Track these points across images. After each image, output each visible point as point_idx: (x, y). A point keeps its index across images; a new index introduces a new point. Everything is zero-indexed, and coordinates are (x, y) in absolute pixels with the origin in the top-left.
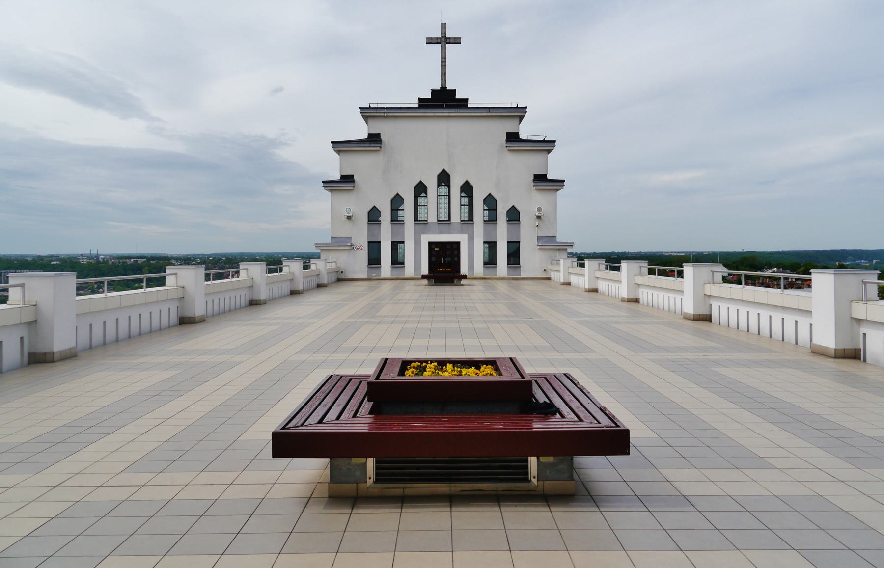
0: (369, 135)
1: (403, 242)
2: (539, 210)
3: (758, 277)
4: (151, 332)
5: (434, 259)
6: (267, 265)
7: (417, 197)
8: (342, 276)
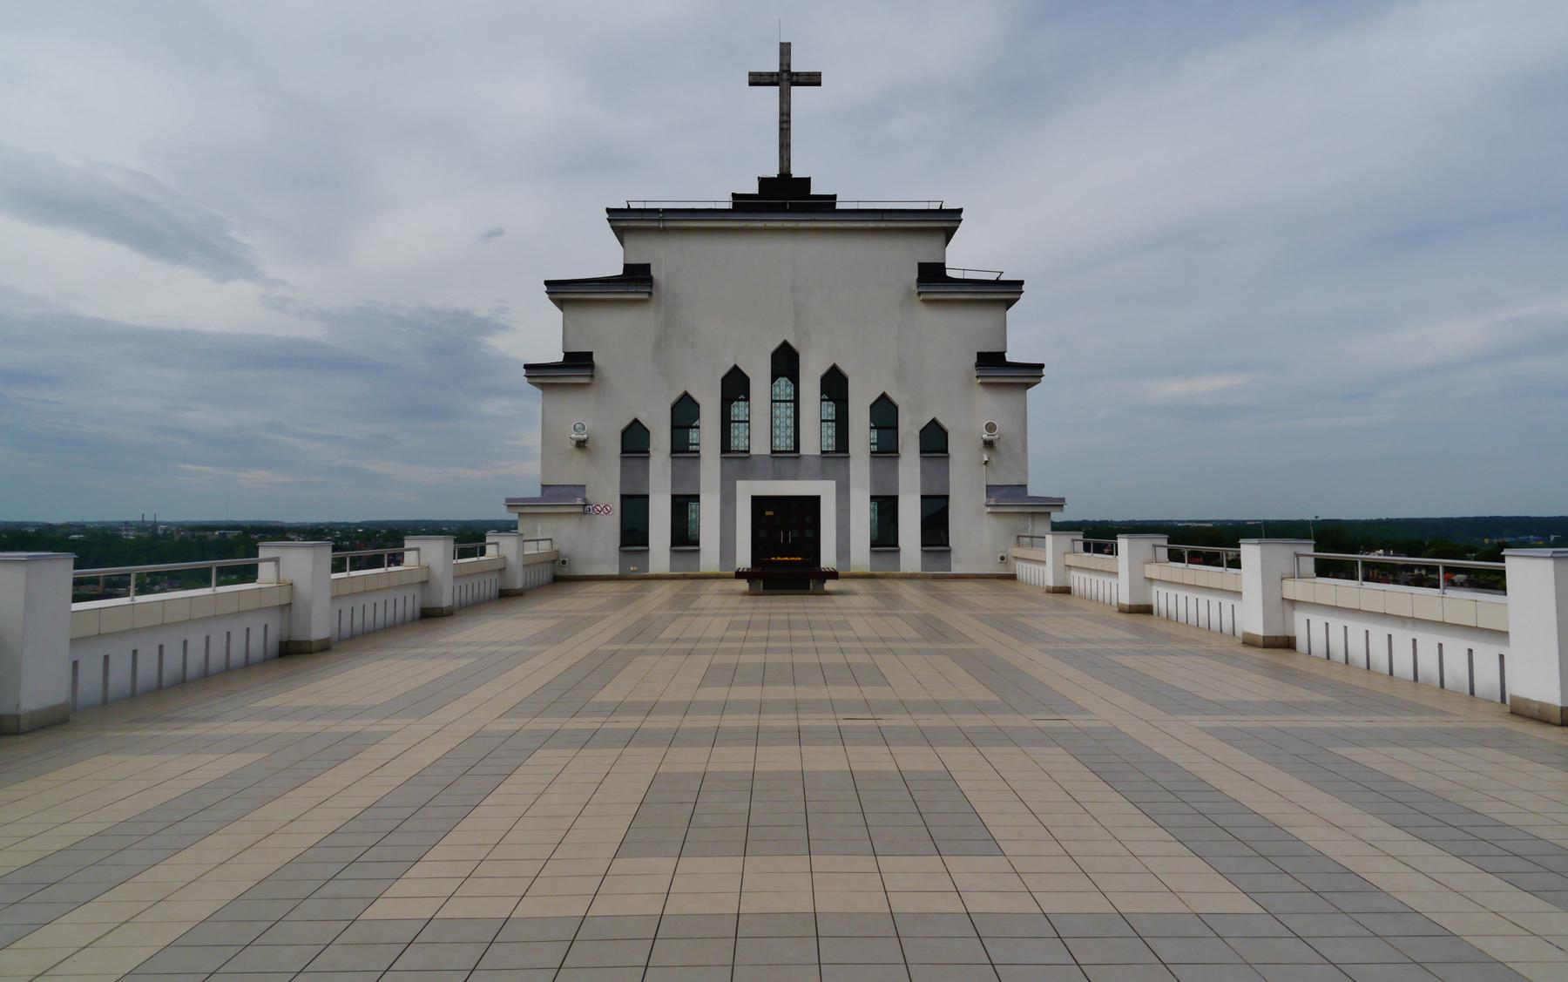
0: (626, 267)
1: (696, 498)
2: (990, 427)
3: (1409, 568)
4: (105, 702)
5: (808, 520)
6: (335, 549)
7: (727, 401)
8: (565, 571)
